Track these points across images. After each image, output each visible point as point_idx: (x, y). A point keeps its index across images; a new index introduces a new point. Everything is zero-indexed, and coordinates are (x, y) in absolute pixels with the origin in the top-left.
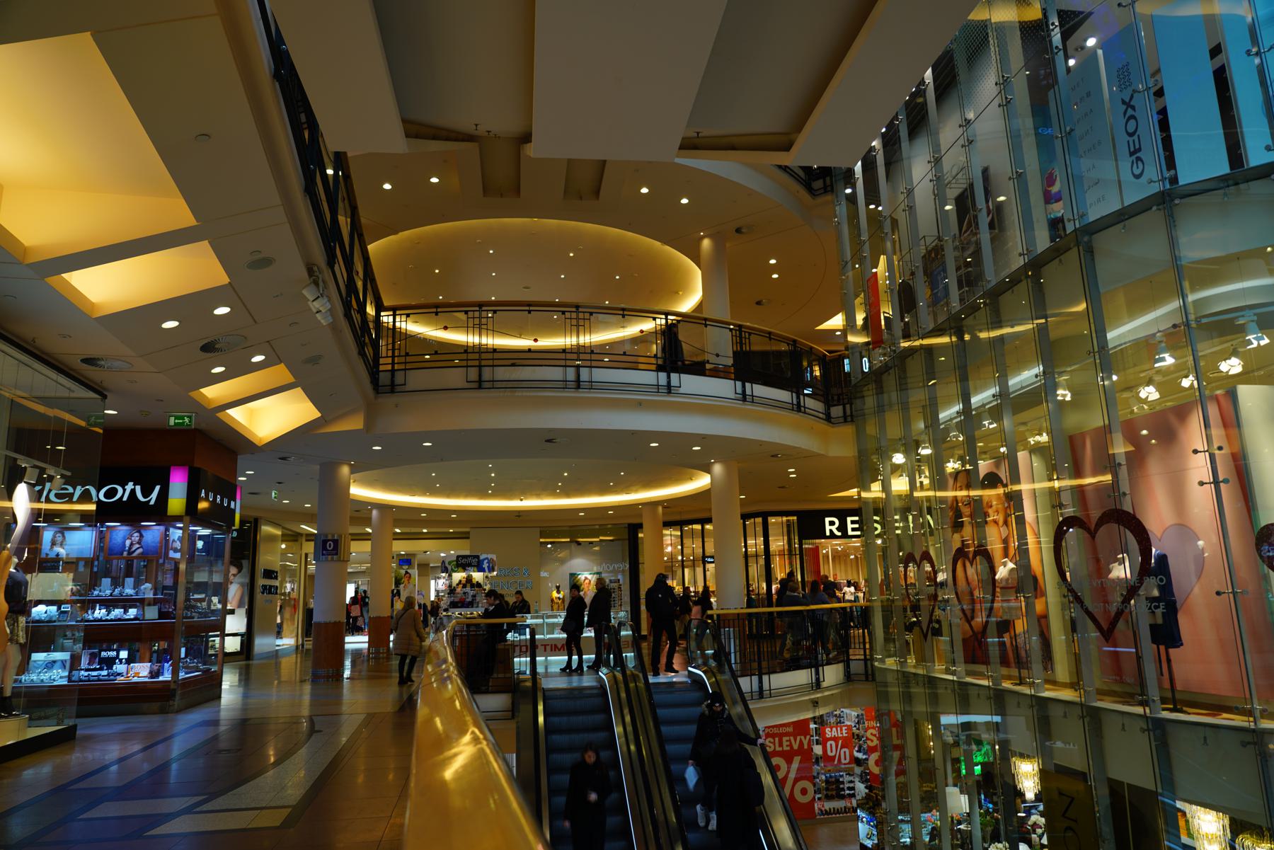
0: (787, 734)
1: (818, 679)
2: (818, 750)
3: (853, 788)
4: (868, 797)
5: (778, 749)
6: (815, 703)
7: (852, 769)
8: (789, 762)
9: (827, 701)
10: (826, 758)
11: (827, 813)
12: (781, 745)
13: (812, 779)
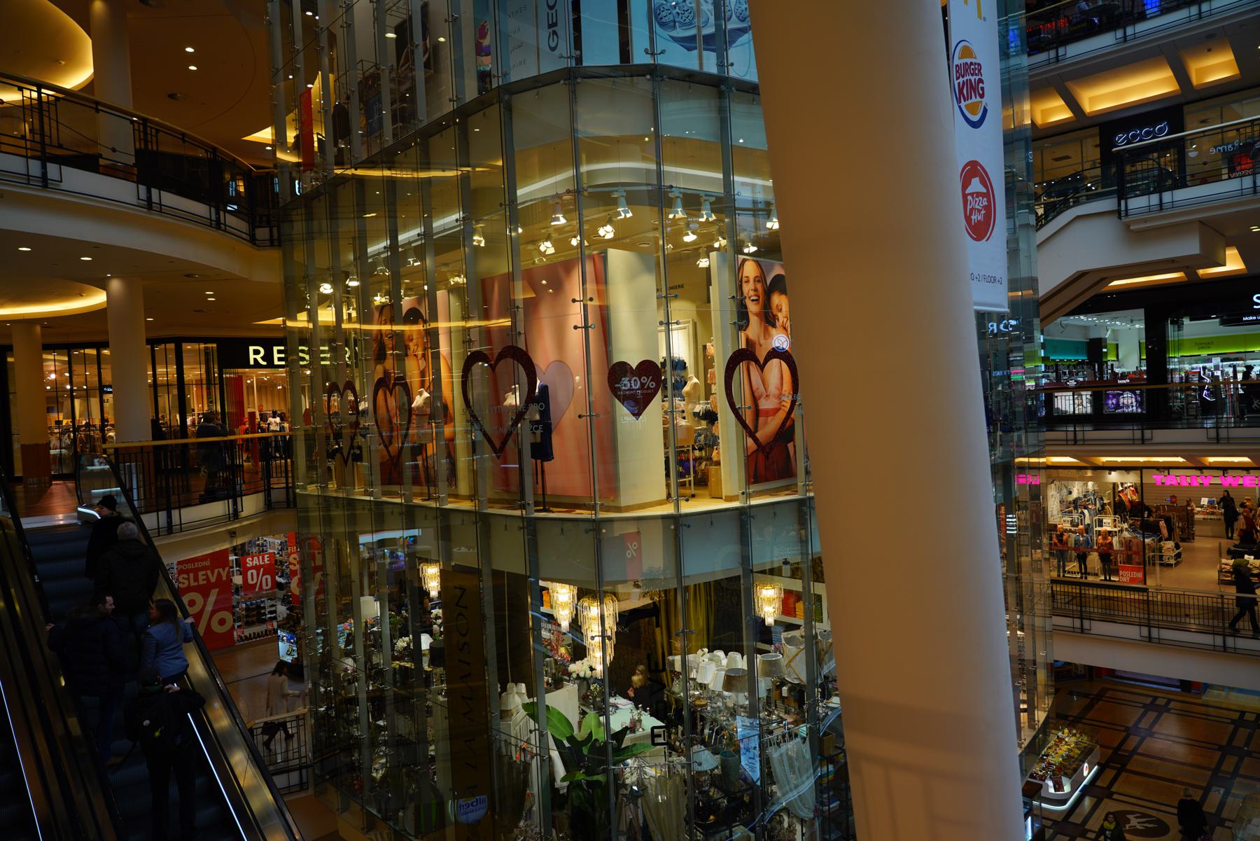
0: (203, 569)
2: (238, 580)
3: (275, 612)
4: (289, 617)
5: (193, 584)
6: (233, 534)
8: (206, 596)
9: (245, 530)
10: (247, 586)
11: (247, 638)
12: (196, 579)
13: (231, 609)
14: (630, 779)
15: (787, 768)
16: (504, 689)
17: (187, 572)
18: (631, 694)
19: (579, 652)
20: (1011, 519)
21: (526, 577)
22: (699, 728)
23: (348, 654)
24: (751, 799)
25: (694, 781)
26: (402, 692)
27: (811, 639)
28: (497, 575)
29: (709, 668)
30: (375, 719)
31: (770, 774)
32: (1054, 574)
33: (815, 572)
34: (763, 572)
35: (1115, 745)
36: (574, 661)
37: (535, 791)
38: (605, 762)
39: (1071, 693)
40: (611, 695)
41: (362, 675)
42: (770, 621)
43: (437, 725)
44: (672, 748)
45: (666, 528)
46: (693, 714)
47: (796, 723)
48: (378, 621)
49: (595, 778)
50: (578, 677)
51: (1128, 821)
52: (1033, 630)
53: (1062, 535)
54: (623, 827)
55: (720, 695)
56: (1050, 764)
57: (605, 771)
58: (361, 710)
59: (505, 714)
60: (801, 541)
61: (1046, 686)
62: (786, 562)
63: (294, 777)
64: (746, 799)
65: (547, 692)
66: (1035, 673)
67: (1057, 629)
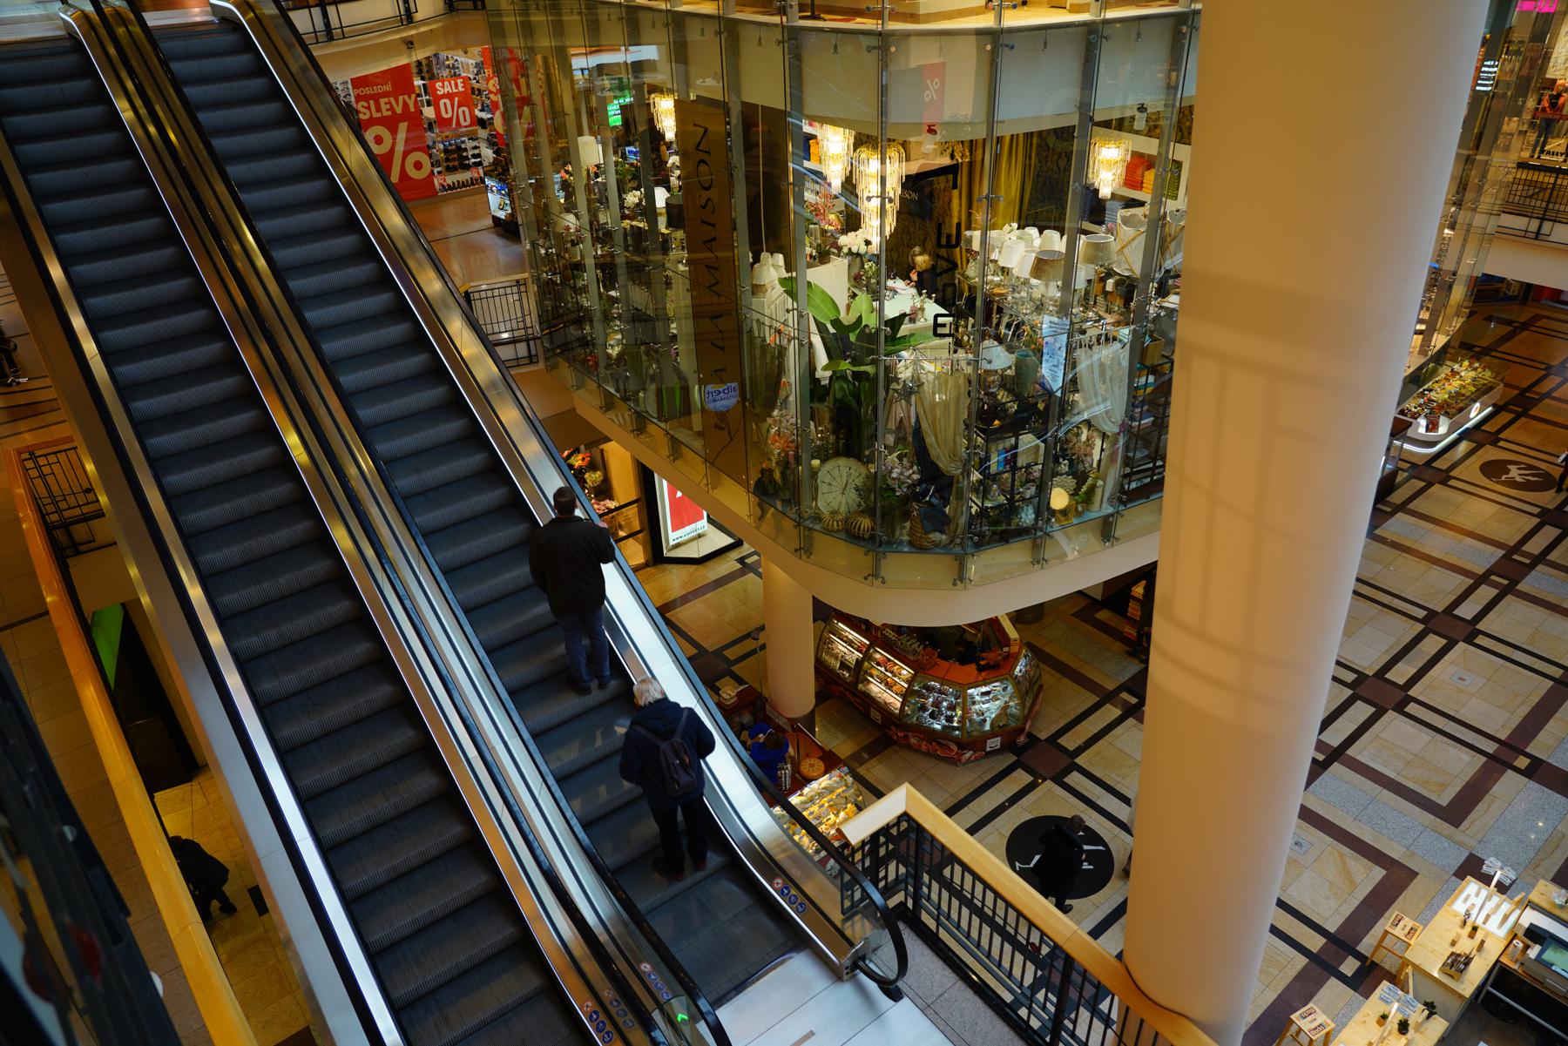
0: (385, 95)
1: (408, 9)
2: (429, 112)
3: (479, 156)
4: (496, 163)
5: (376, 115)
6: (409, 44)
7: (475, 132)
8: (394, 131)
9: (426, 39)
10: (442, 122)
11: (450, 188)
12: (378, 109)
13: (427, 149)
14: (904, 373)
15: (1096, 375)
16: (757, 259)
17: (366, 98)
18: (914, 277)
19: (852, 221)
20: (1491, 68)
21: (785, 114)
22: (995, 321)
23: (570, 207)
24: (1047, 407)
25: (980, 381)
26: (637, 259)
27: (1158, 222)
28: (749, 111)
29: (1013, 250)
30: (607, 288)
31: (1074, 381)
32: (1526, 154)
33: (1180, 129)
34: (1106, 124)
35: (1524, 385)
36: (845, 231)
37: (792, 380)
38: (875, 352)
39: (1489, 319)
40: (889, 277)
41: (587, 235)
42: (1105, 192)
43: (678, 300)
44: (958, 344)
45: (980, 48)
46: (988, 304)
47: (1117, 324)
48: (599, 170)
49: (862, 368)
50: (850, 253)
51: (1508, 471)
52: (1468, 231)
53: (1559, 95)
54: (892, 425)
55: (1026, 282)
56: (1430, 400)
57: (875, 362)
58: (590, 277)
59: (757, 289)
60: (1169, 87)
61: (1460, 306)
62: (1142, 108)
63: (522, 349)
64: (1041, 406)
65: (809, 266)
66: (1451, 287)
67: (1503, 233)
